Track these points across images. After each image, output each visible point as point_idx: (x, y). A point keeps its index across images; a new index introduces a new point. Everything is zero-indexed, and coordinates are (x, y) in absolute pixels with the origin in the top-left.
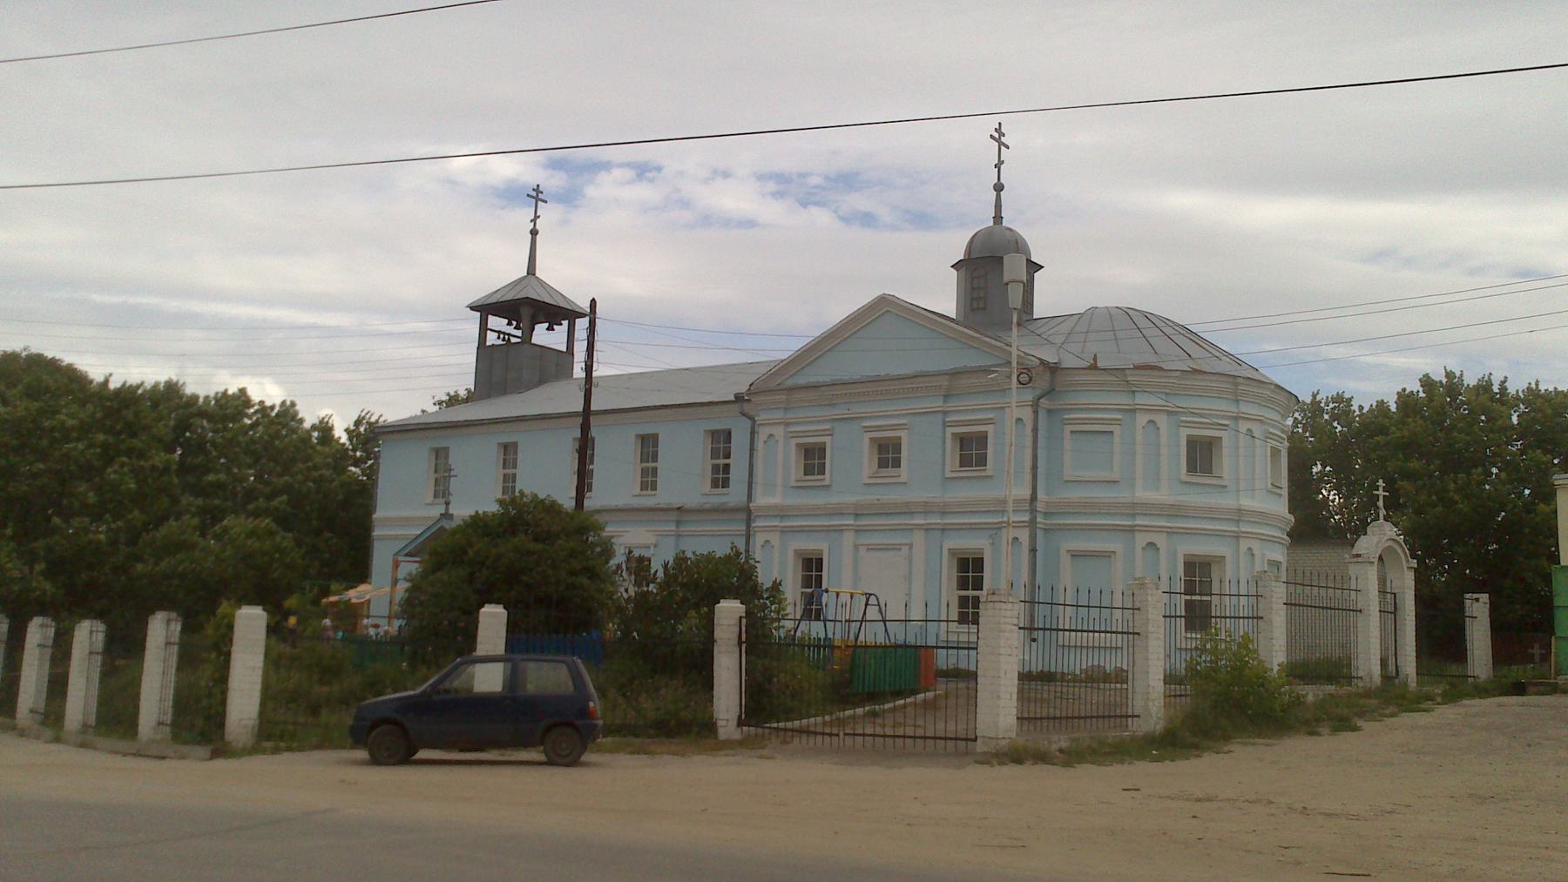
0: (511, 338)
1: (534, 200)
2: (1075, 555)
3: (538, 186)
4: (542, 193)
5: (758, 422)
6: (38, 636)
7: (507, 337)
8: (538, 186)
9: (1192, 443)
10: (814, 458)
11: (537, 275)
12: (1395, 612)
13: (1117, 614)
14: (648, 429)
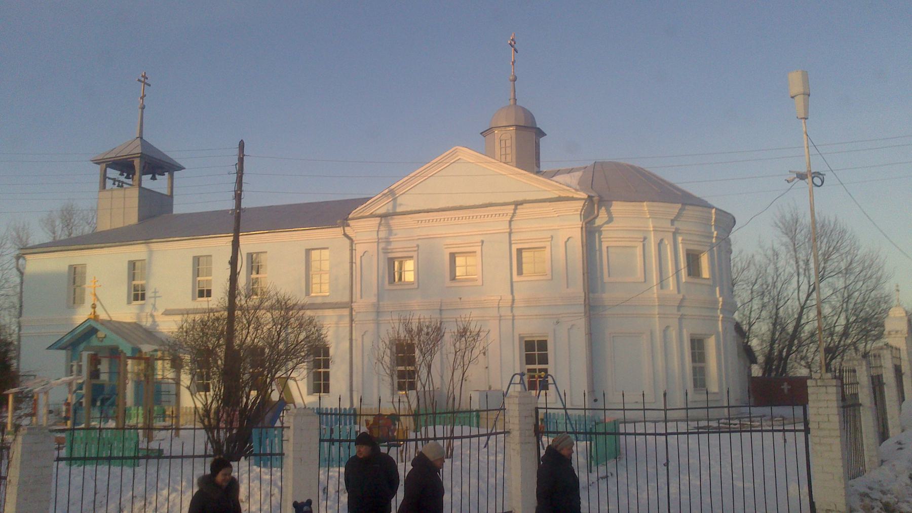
0: (124, 185)
4: (147, 79)
5: (355, 242)
7: (121, 184)
11: (144, 138)
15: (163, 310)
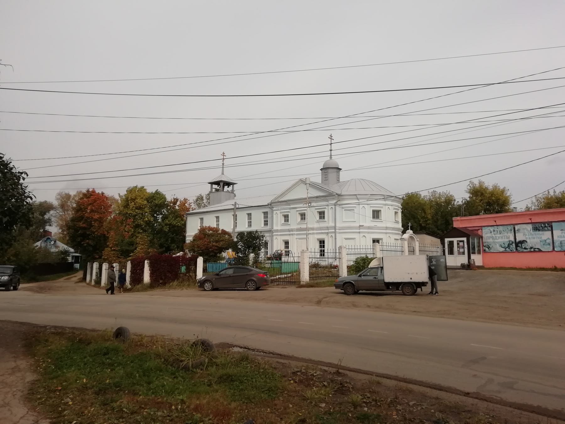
1: (223, 156)
6: (105, 267)
9: (374, 211)
10: (286, 217)
12: (414, 252)
13: (399, 247)
14: (217, 215)
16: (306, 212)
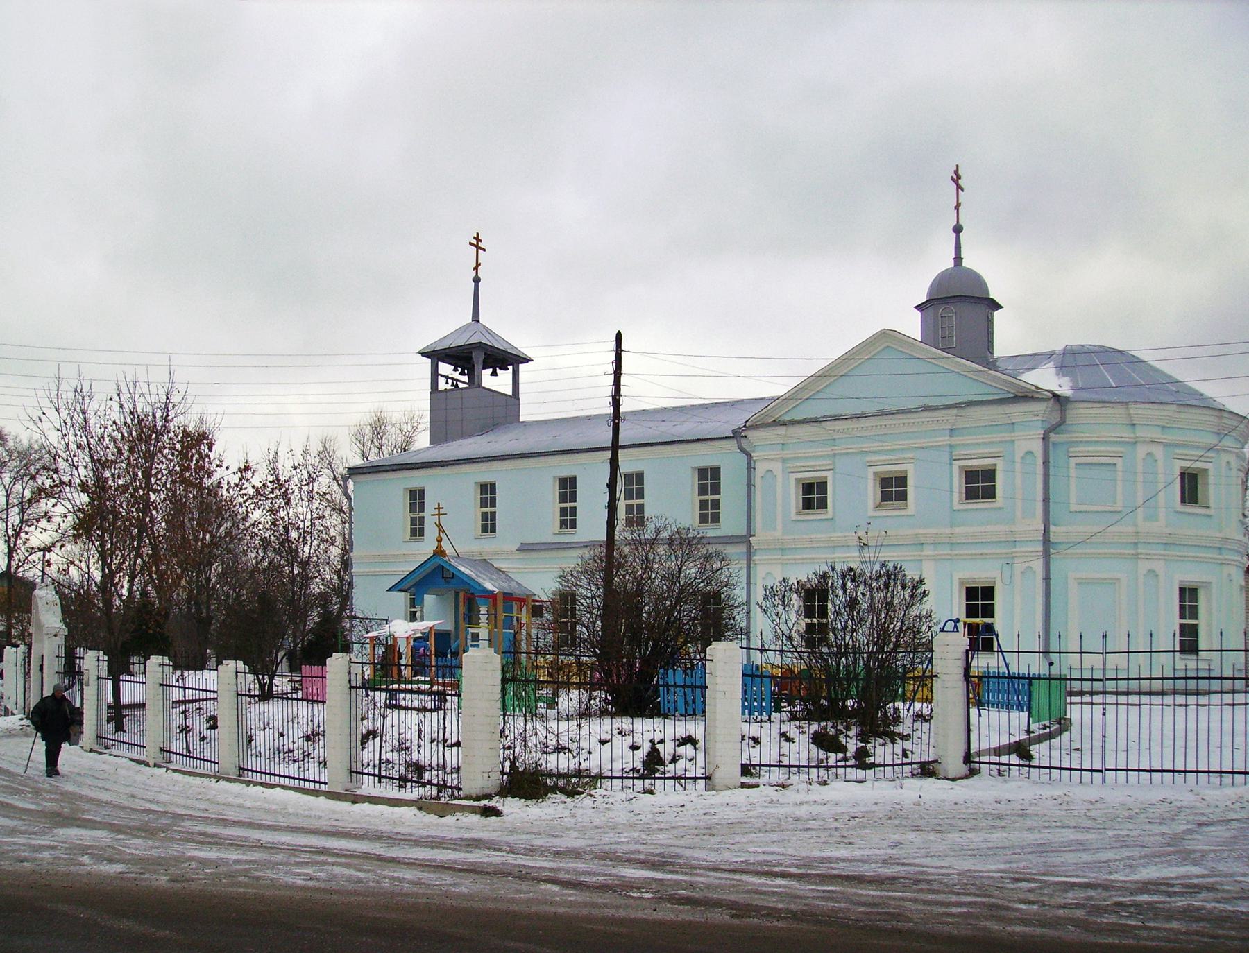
2: (1082, 582)
3: (478, 234)
7: (455, 382)
8: (478, 234)
14: (416, 484)
15: (519, 545)
16: (829, 474)
